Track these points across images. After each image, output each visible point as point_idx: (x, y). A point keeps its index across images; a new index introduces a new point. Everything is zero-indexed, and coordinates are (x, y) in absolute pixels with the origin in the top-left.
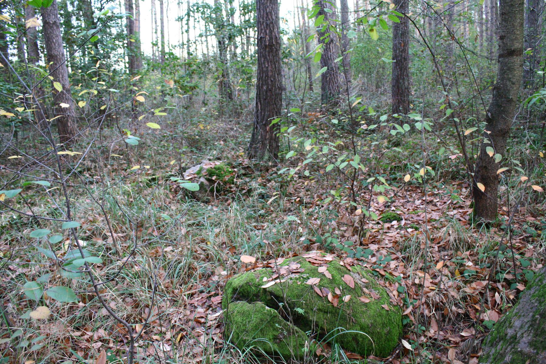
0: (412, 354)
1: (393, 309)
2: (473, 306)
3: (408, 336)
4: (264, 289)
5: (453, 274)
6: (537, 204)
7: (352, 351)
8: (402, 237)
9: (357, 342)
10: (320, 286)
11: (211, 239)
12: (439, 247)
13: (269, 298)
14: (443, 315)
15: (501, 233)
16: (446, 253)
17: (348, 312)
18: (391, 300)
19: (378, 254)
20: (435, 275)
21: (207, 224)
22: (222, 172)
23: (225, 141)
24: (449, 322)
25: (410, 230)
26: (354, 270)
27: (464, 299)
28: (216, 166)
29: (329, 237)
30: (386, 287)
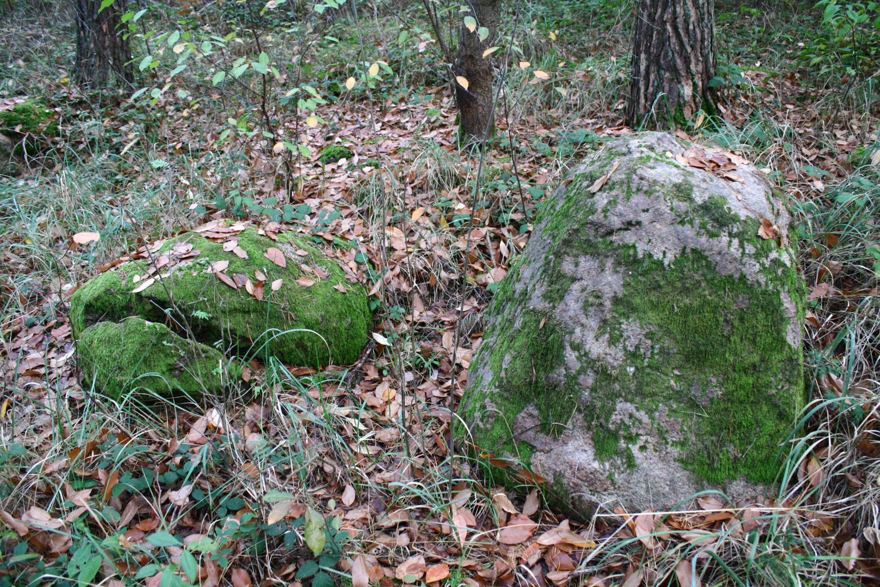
0: (391, 352)
1: (351, 289)
2: (470, 267)
3: (380, 326)
4: (138, 294)
5: (436, 224)
6: (549, 109)
7: (299, 365)
8: (355, 182)
9: (304, 349)
10: (230, 273)
11: (32, 233)
12: (412, 188)
13: (148, 307)
14: (430, 288)
15: (503, 157)
16: (424, 195)
17: (283, 305)
18: (347, 277)
19: (319, 213)
20: (412, 231)
21: (20, 208)
22: (33, 116)
23: (26, 60)
24: (439, 295)
25: (367, 169)
26: (282, 240)
27: (457, 258)
28: (17, 107)
29: (237, 195)
30: (337, 258)
